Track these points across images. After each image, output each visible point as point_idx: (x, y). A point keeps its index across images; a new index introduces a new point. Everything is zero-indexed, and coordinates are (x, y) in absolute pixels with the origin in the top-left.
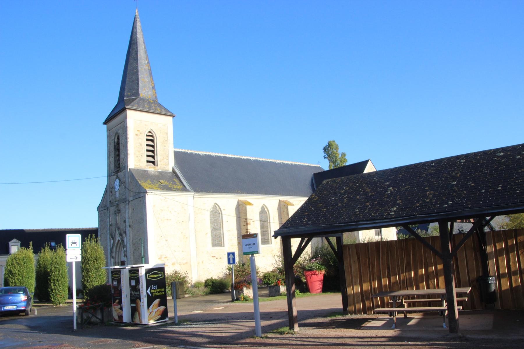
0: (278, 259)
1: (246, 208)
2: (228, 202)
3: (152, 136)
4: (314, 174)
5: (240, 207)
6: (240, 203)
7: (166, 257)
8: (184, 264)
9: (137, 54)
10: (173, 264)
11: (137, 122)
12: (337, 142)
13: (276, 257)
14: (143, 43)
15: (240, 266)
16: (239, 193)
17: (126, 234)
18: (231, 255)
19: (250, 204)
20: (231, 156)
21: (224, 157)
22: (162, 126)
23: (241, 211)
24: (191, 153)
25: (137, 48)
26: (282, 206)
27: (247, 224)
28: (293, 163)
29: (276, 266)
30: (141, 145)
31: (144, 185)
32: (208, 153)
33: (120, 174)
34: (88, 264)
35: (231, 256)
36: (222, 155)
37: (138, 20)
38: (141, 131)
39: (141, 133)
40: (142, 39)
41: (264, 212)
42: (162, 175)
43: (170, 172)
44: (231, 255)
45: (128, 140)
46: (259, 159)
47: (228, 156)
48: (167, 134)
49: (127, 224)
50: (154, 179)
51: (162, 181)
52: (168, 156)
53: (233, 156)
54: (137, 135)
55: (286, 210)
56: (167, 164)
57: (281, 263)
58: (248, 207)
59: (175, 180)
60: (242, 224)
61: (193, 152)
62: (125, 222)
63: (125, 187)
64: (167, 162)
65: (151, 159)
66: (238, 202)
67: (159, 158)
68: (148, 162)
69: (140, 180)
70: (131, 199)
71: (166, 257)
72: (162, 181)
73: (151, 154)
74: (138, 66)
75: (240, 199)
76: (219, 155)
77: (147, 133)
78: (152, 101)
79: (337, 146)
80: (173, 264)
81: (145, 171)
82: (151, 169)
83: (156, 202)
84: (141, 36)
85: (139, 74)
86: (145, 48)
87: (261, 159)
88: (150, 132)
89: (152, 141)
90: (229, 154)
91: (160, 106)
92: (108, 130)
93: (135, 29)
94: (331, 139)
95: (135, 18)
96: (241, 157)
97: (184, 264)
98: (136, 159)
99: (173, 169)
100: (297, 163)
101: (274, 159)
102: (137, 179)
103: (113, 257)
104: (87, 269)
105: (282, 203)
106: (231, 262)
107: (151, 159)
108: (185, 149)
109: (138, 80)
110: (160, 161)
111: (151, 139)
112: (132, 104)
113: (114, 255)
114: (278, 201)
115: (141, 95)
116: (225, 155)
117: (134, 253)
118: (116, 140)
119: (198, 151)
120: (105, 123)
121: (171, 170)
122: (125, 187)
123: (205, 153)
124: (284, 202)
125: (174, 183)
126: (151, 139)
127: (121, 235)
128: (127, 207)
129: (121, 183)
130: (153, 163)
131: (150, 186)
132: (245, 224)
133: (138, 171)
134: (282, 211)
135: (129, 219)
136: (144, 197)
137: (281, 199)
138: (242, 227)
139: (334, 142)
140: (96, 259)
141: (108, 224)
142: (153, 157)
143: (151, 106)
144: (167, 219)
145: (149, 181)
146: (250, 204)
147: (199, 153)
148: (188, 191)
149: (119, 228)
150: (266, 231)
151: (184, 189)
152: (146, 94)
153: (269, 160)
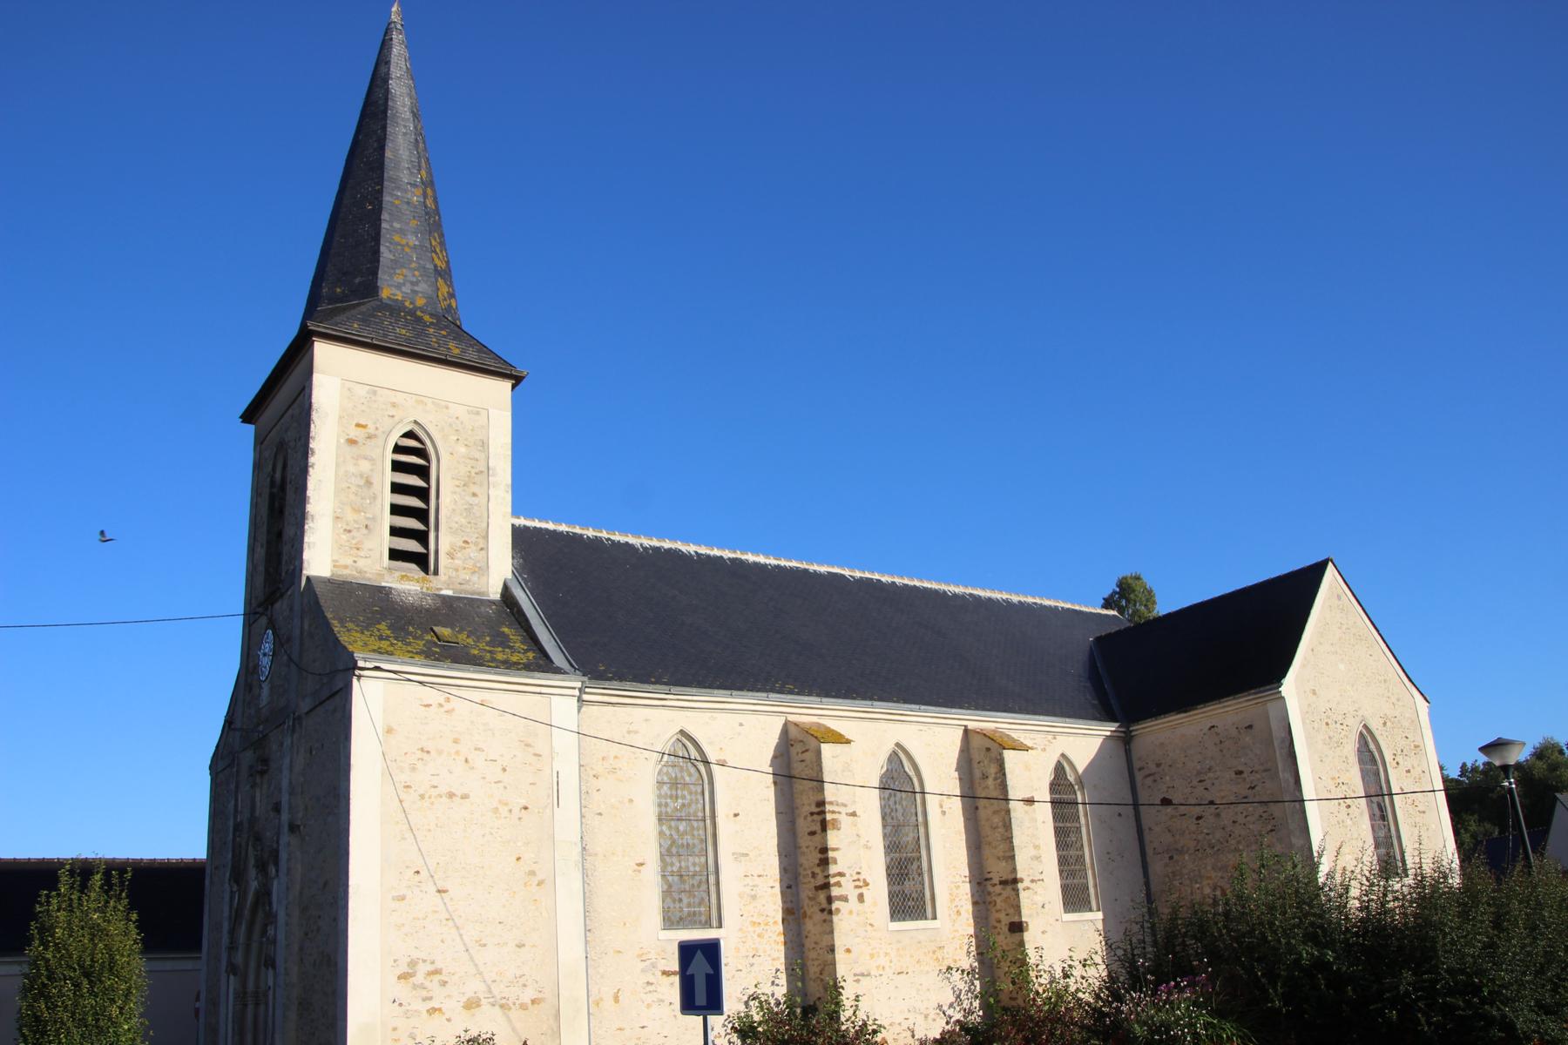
0: (962, 986)
1: (819, 753)
2: (740, 731)
3: (421, 453)
4: (1098, 640)
5: (793, 751)
6: (793, 732)
7: (437, 972)
8: (523, 1007)
9: (382, 148)
10: (471, 1005)
11: (357, 394)
12: (1149, 580)
13: (957, 976)
14: (408, 115)
15: (792, 1013)
16: (791, 692)
17: (276, 864)
18: (699, 955)
19: (839, 739)
20: (762, 559)
21: (733, 560)
22: (470, 416)
23: (797, 772)
24: (597, 540)
25: (384, 128)
26: (976, 756)
27: (824, 826)
28: (1015, 599)
29: (958, 1016)
30: (369, 483)
31: (352, 638)
32: (667, 545)
33: (280, 606)
34: (48, 998)
35: (700, 965)
36: (727, 554)
37: (397, 38)
38: (371, 430)
39: (370, 437)
40: (407, 101)
41: (899, 783)
42: (454, 609)
43: (493, 602)
44: (699, 955)
45: (312, 460)
46: (876, 576)
47: (750, 558)
48: (484, 445)
49: (285, 817)
50: (410, 623)
51: (445, 631)
52: (486, 537)
53: (772, 561)
54: (352, 442)
55: (992, 770)
56: (483, 569)
57: (976, 1004)
58: (827, 750)
59: (506, 630)
60: (804, 825)
61: (604, 535)
62: (277, 808)
63: (290, 659)
64: (479, 554)
65: (412, 546)
66: (785, 731)
67: (445, 541)
68: (395, 555)
69: (342, 622)
70: (305, 706)
71: (437, 972)
72: (445, 631)
73: (412, 523)
74: (381, 192)
75: (791, 718)
76: (716, 552)
77: (394, 438)
78: (427, 318)
79: (1150, 592)
80: (471, 1005)
81: (380, 593)
82: (407, 583)
83: (392, 714)
84: (405, 90)
85: (385, 216)
86: (418, 133)
87: (886, 579)
88: (410, 435)
89: (423, 472)
90: (756, 552)
91: (459, 333)
92: (260, 441)
93: (383, 69)
94: (1126, 571)
95: (388, 31)
96: (804, 566)
97: (523, 1007)
98: (341, 539)
99: (506, 588)
100: (1030, 600)
101: (938, 581)
102: (329, 615)
103: (232, 969)
104: (37, 1019)
105: (976, 742)
106: (701, 999)
107: (412, 546)
108: (568, 523)
109: (377, 238)
110: (451, 555)
111: (413, 461)
112: (338, 319)
113: (239, 958)
114: (960, 732)
115: (385, 293)
116: (738, 555)
117: (301, 949)
118: (278, 475)
119: (624, 532)
120: (248, 416)
121: (495, 593)
122: (290, 659)
123: (655, 543)
124: (983, 734)
125: (504, 642)
126: (413, 461)
127: (262, 867)
128: (287, 742)
129: (280, 643)
130: (421, 561)
131: (384, 644)
132: (817, 828)
133: (343, 588)
134: (977, 774)
135: (292, 793)
136: (347, 691)
137: (971, 725)
138: (804, 841)
139: (1138, 578)
140: (87, 975)
141: (231, 823)
142: (422, 537)
143: (421, 334)
144: (451, 795)
145: (383, 626)
146: (839, 739)
147: (631, 540)
148: (558, 671)
149: (258, 838)
150: (910, 860)
151: (543, 664)
152: (407, 289)
153: (918, 584)
